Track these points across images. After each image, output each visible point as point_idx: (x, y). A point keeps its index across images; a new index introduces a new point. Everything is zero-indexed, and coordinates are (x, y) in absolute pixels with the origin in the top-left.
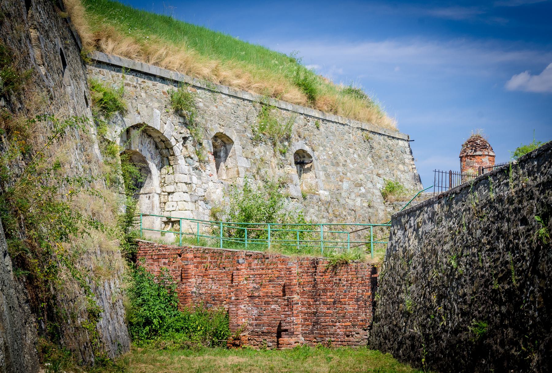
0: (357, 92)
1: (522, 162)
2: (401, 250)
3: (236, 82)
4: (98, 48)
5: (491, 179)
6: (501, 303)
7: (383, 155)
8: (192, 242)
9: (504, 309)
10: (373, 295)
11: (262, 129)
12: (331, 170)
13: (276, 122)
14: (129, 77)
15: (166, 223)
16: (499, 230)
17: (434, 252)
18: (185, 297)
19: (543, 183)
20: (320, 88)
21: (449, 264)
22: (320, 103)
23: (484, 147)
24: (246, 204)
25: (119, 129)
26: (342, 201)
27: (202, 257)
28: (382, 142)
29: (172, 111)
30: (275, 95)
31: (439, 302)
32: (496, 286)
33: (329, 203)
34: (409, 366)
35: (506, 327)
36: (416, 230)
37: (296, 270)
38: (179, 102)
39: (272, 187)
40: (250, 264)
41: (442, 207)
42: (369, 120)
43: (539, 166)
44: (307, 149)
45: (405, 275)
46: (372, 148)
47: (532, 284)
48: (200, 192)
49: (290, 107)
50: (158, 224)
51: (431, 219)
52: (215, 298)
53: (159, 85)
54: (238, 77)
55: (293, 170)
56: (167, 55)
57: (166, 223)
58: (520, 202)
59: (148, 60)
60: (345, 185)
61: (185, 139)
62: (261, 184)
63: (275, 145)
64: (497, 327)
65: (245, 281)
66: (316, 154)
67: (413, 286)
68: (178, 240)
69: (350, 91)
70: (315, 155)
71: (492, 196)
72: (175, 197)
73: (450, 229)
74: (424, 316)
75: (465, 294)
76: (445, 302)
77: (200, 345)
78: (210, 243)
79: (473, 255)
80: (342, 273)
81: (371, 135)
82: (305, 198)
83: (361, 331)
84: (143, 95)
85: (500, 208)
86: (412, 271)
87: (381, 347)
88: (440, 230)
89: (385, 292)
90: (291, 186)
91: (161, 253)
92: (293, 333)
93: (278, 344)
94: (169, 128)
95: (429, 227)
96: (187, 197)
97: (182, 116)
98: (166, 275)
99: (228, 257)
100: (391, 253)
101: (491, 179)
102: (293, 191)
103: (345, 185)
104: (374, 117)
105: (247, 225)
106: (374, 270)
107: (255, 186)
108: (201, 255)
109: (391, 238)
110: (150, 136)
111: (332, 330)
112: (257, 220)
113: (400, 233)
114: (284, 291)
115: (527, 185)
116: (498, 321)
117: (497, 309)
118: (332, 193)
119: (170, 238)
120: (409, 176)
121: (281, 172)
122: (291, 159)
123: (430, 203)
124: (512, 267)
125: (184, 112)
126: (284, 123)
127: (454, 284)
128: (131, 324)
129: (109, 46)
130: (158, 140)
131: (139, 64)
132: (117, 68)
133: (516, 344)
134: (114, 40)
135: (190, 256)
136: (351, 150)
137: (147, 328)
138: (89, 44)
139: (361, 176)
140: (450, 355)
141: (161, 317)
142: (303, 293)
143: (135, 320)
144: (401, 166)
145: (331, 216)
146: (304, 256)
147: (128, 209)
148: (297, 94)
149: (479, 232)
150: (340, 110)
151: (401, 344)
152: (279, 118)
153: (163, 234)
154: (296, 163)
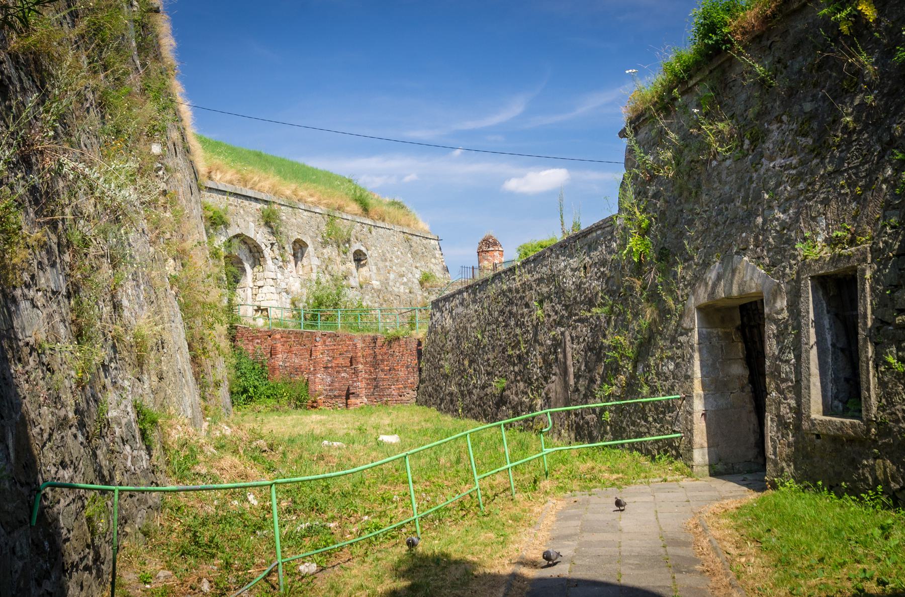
0: (399, 204)
1: (524, 264)
2: (439, 327)
3: (310, 199)
4: (210, 178)
5: (503, 275)
6: (514, 365)
7: (420, 252)
8: (277, 325)
9: (516, 369)
10: (419, 363)
11: (329, 235)
12: (381, 264)
13: (340, 229)
14: (232, 198)
15: (257, 311)
16: (510, 312)
17: (465, 328)
18: (273, 370)
19: (538, 279)
20: (372, 202)
21: (476, 337)
22: (372, 214)
23: (495, 244)
24: (318, 293)
25: (223, 239)
26: (390, 289)
27: (287, 338)
28: (418, 241)
29: (262, 223)
30: (339, 209)
31: (470, 366)
32: (510, 352)
33: (380, 290)
34: (449, 415)
35: (518, 381)
36: (451, 312)
37: (360, 345)
38: (268, 216)
39: (337, 280)
40: (324, 342)
41: (469, 295)
42: (408, 226)
43: (535, 267)
44: (363, 249)
45: (443, 346)
46: (411, 246)
47: (535, 350)
48: (283, 285)
49: (350, 218)
50: (250, 311)
51: (462, 304)
52: (297, 370)
53: (254, 204)
54: (311, 196)
55: (352, 265)
56: (259, 181)
57: (257, 311)
58: (524, 292)
59: (246, 186)
60: (392, 276)
61: (272, 244)
62: (328, 277)
63: (339, 247)
64: (512, 383)
65: (321, 355)
66: (370, 252)
67: (450, 355)
68: (266, 324)
69: (394, 203)
70: (369, 253)
71: (505, 287)
72: (264, 290)
73: (476, 311)
74: (459, 377)
75: (489, 359)
76: (474, 365)
77: (286, 407)
78: (291, 325)
79: (493, 330)
80: (395, 345)
81: (410, 237)
82: (361, 287)
83: (411, 392)
84: (242, 212)
85: (510, 296)
86: (449, 343)
87: (426, 403)
88: (469, 312)
89: (428, 360)
90: (351, 278)
91: (254, 335)
92: (358, 395)
93: (347, 404)
94: (261, 236)
95: (460, 309)
96: (273, 289)
97: (270, 227)
98: (259, 351)
99: (307, 337)
100: (432, 330)
101: (503, 275)
102: (353, 282)
103: (392, 276)
104: (412, 223)
105: (320, 309)
106: (420, 344)
107: (325, 279)
108: (286, 335)
109: (431, 319)
110: (245, 243)
111: (388, 392)
112: (327, 306)
113: (438, 314)
114: (351, 362)
115: (528, 280)
116: (512, 377)
117: (512, 369)
118: (382, 283)
119: (260, 322)
120: (439, 268)
121: (343, 268)
122: (351, 257)
123: (460, 292)
124: (520, 338)
125: (272, 224)
126: (345, 230)
127: (481, 352)
128: (232, 393)
129: (217, 176)
130: (251, 246)
131: (239, 189)
132: (223, 192)
133: (526, 393)
134: (221, 172)
135: (278, 336)
136: (396, 249)
137: (245, 396)
138: (203, 175)
139: (404, 269)
140: (479, 405)
141: (255, 387)
142: (366, 363)
143: (235, 390)
144: (433, 260)
145: (382, 301)
146: (367, 333)
147: (230, 300)
148: (355, 207)
149: (497, 313)
150: (387, 218)
151: (442, 400)
152: (342, 225)
153: (254, 319)
154: (355, 260)
